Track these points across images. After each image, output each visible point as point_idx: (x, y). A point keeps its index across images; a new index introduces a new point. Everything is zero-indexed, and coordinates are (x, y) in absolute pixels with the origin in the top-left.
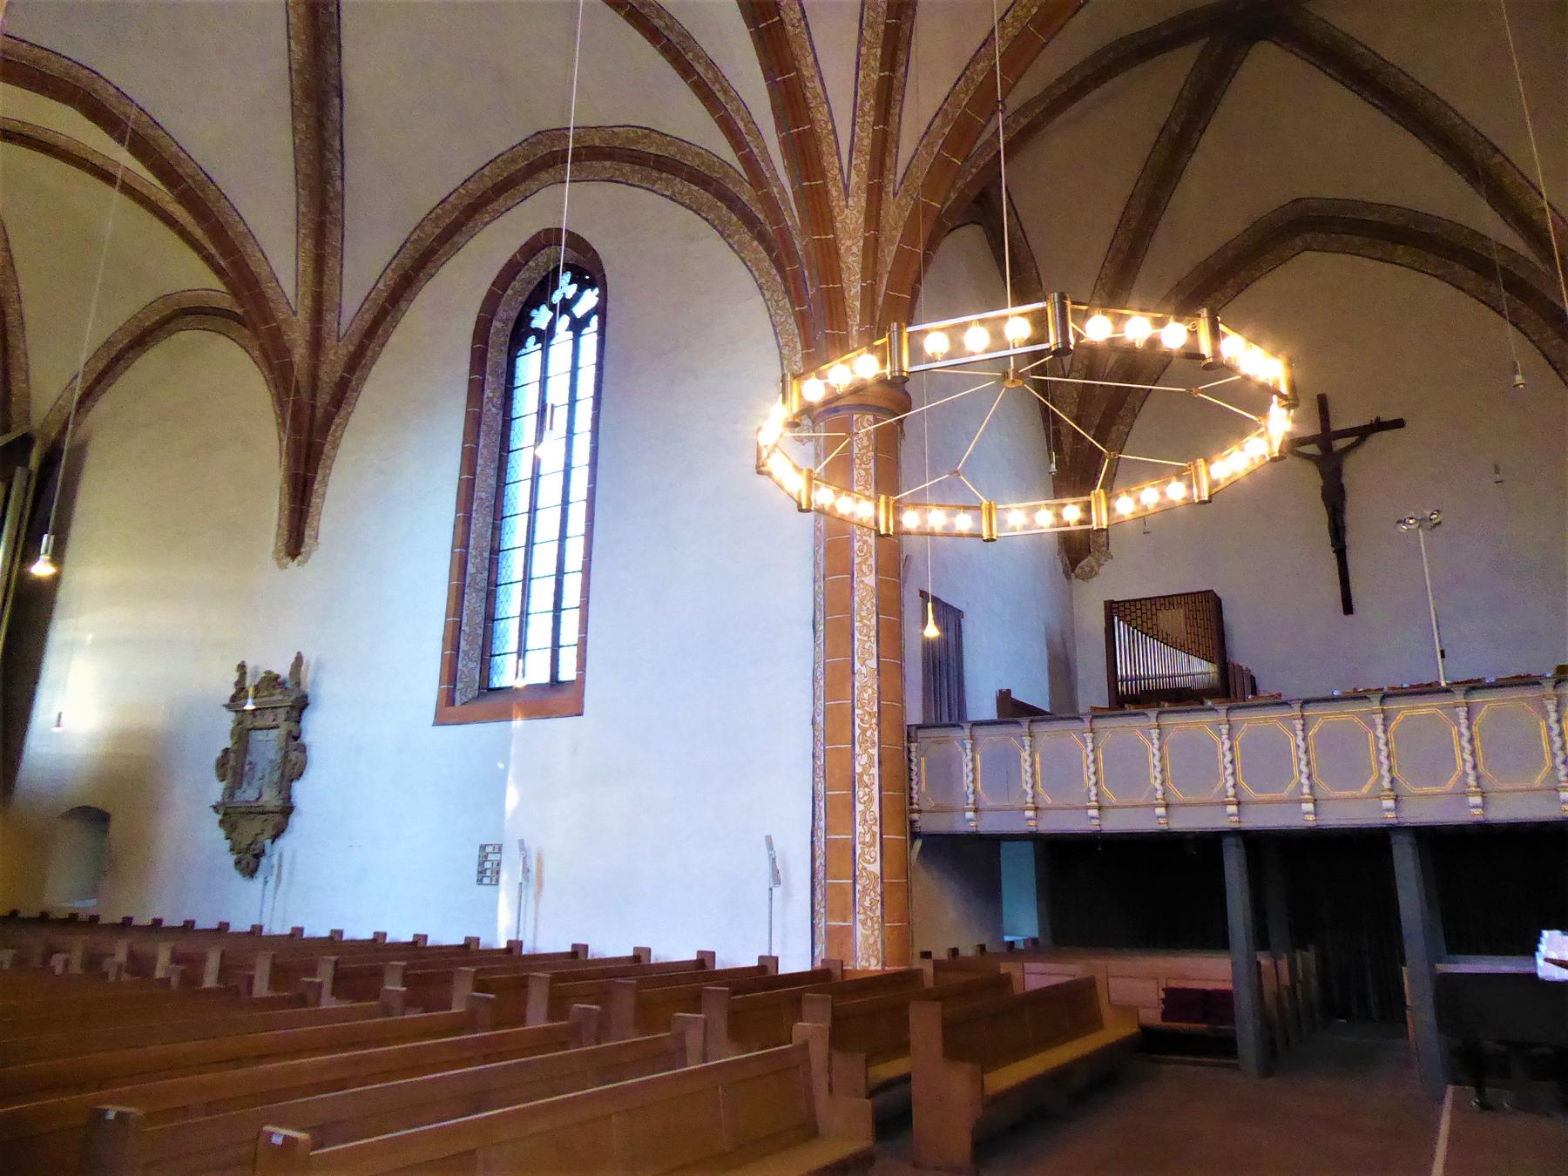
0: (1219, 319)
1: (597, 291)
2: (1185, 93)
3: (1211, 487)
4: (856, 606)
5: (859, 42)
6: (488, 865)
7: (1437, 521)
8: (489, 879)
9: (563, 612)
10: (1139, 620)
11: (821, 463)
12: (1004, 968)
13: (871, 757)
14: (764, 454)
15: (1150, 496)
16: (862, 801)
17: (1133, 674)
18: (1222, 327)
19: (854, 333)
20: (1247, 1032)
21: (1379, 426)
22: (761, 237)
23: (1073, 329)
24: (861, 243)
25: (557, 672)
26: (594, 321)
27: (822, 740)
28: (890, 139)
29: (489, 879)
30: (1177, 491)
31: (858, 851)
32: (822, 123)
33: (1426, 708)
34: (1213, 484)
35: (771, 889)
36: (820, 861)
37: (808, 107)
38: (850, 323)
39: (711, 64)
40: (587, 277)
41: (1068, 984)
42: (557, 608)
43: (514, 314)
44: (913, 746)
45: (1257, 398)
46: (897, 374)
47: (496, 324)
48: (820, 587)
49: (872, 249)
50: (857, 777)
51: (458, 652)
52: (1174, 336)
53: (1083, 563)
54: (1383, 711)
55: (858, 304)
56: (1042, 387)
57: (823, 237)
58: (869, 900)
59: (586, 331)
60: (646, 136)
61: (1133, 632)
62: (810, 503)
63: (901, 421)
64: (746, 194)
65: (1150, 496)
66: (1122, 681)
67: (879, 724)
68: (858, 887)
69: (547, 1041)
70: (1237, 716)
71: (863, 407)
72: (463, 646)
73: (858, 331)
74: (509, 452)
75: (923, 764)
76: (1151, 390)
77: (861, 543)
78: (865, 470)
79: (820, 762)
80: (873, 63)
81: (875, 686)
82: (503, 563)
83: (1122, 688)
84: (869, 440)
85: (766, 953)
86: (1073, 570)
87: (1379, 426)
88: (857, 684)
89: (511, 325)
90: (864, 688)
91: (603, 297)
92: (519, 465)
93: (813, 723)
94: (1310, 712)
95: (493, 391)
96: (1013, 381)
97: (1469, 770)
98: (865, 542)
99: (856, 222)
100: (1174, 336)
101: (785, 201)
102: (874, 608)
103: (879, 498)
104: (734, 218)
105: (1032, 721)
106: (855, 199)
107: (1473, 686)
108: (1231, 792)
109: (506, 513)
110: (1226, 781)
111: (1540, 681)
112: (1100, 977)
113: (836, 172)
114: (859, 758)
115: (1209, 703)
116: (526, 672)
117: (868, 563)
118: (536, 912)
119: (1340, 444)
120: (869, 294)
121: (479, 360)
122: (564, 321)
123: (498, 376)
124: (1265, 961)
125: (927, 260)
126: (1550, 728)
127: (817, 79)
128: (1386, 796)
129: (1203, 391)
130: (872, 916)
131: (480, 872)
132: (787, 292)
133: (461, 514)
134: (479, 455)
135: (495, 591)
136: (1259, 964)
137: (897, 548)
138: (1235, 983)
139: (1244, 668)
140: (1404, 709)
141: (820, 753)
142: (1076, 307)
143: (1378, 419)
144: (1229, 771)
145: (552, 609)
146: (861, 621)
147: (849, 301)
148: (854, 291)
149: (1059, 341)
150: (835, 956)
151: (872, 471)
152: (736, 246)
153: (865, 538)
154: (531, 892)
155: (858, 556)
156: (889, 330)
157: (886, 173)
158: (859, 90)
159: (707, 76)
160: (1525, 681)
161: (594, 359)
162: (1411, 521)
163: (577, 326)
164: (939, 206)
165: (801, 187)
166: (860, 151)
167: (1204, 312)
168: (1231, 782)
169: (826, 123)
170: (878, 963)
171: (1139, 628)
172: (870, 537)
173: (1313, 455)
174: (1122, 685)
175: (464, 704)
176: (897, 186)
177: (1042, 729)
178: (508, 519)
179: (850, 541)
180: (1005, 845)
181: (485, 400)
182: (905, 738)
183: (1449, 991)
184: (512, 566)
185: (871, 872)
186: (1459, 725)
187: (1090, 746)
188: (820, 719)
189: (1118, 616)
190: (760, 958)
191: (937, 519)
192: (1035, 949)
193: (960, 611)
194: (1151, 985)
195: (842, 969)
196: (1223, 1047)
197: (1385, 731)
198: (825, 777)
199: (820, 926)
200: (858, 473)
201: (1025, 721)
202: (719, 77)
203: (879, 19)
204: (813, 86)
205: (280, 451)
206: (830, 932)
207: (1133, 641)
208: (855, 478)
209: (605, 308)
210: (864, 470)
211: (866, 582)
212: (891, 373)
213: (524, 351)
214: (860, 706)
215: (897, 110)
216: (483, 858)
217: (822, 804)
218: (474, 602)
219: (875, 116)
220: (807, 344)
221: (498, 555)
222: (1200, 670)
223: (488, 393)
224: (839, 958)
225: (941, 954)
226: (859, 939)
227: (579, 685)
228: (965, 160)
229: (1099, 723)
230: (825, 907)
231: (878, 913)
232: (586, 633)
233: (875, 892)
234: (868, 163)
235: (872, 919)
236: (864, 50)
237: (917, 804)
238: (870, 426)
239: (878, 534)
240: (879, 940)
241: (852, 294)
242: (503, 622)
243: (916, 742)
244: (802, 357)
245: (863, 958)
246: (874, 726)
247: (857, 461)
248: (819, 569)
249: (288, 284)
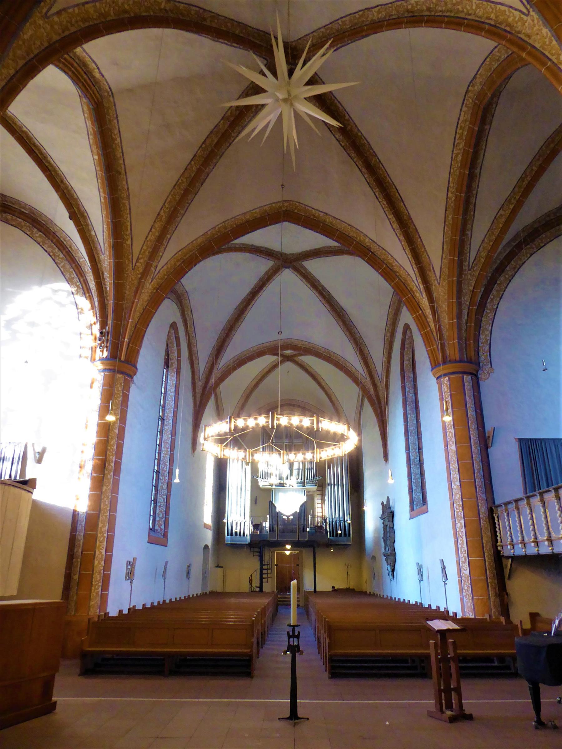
13: (461, 524)
51: (412, 490)
67: (463, 509)
68: (463, 581)
72: (414, 487)
81: (460, 493)
88: (454, 493)
90: (456, 494)
98: (450, 432)
113: (415, 287)
185: (465, 574)
231: (470, 592)
233: (468, 583)
246: (461, 510)
249: (361, 371)
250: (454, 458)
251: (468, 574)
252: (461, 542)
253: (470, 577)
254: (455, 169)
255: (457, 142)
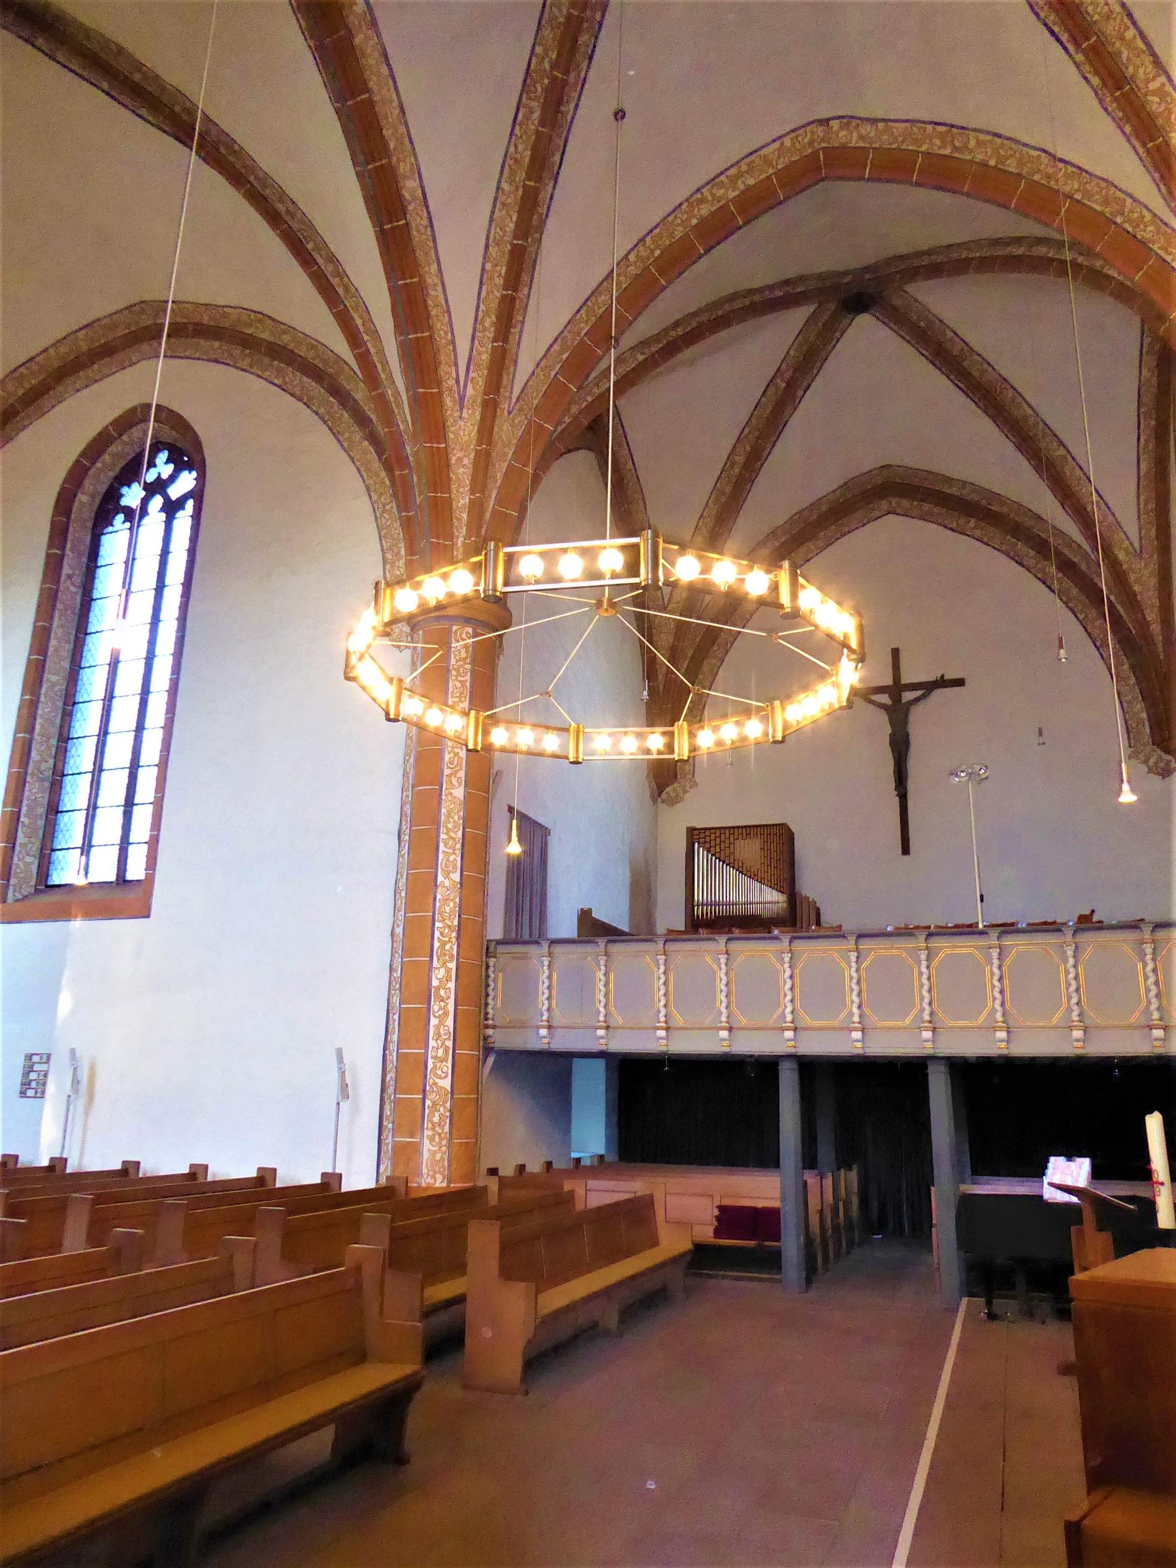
0: (799, 571)
1: (194, 474)
2: (792, 353)
3: (785, 728)
4: (443, 818)
5: (484, 258)
6: (33, 1076)
7: (984, 776)
8: (34, 1090)
9: (135, 807)
10: (718, 847)
11: (416, 670)
12: (567, 1186)
13: (448, 971)
14: (353, 660)
15: (729, 731)
16: (437, 1015)
17: (705, 898)
18: (801, 580)
19: (460, 544)
20: (791, 1245)
21: (942, 683)
22: (373, 439)
23: (663, 564)
24: (472, 456)
25: (125, 870)
26: (190, 504)
27: (400, 952)
28: (508, 357)
29: (34, 1090)
30: (754, 729)
31: (430, 1065)
32: (442, 333)
33: (965, 947)
34: (786, 726)
35: (338, 1104)
36: (390, 1075)
37: (428, 317)
38: (456, 534)
39: (332, 258)
40: (186, 459)
41: (628, 1201)
42: (129, 804)
43: (103, 488)
44: (492, 961)
45: (832, 647)
46: (490, 592)
47: (82, 498)
48: (407, 796)
49: (483, 462)
50: (433, 990)
51: (14, 844)
52: (757, 583)
53: (668, 789)
54: (927, 948)
55: (465, 516)
56: (640, 620)
57: (435, 445)
58: (437, 1114)
59: (180, 514)
60: (260, 321)
61: (711, 859)
62: (398, 714)
63: (501, 636)
64: (360, 393)
65: (729, 731)
66: (698, 905)
67: (458, 938)
68: (428, 1103)
69: (84, 1268)
70: (799, 945)
71: (467, 621)
72: (21, 838)
73: (464, 543)
74: (87, 634)
75: (500, 980)
76: (740, 632)
77: (452, 755)
78: (461, 682)
79: (397, 974)
80: (497, 280)
81: (457, 900)
82: (73, 751)
83: (698, 911)
84: (467, 652)
85: (330, 1170)
86: (660, 795)
87: (942, 683)
88: (439, 896)
89: (98, 501)
90: (446, 900)
91: (201, 479)
92: (96, 649)
93: (392, 935)
94: (865, 945)
95: (71, 567)
96: (606, 610)
97: (998, 1007)
98: (456, 754)
99: (469, 435)
100: (757, 583)
101: (400, 405)
102: (461, 821)
103: (690, 751)
104: (346, 415)
105: (609, 941)
106: (470, 412)
107: (1008, 928)
108: (789, 1018)
109: (79, 698)
110: (786, 1007)
111: (1063, 929)
112: (659, 1196)
113: (452, 382)
114: (437, 971)
115: (776, 932)
116: (90, 870)
117: (458, 776)
118: (85, 1127)
119: (908, 696)
120: (477, 508)
121: (59, 534)
122: (157, 502)
123: (80, 555)
124: (811, 1178)
125: (536, 479)
126: (1067, 972)
127: (439, 288)
128: (925, 1027)
129: (781, 638)
130: (440, 1131)
131: (23, 1084)
132: (395, 495)
133: (27, 697)
134: (53, 635)
135: (61, 782)
136: (805, 1183)
137: (489, 763)
138: (783, 1199)
139: (811, 900)
140: (946, 947)
141: (397, 965)
142: (668, 545)
143: (942, 676)
144: (789, 998)
145: (123, 803)
146: (447, 834)
147: (456, 514)
148: (462, 502)
149: (650, 576)
150: (401, 1172)
151: (468, 684)
152: (345, 444)
153: (456, 750)
154: (81, 1103)
155: (448, 767)
156: (486, 549)
157: (502, 390)
158: (481, 305)
159: (328, 269)
160: (1050, 927)
161: (186, 544)
162: (962, 774)
163: (171, 508)
164: (552, 429)
165: (416, 393)
166: (479, 366)
167: (786, 564)
168: (789, 1009)
169: (446, 333)
170: (444, 1178)
171: (717, 855)
172: (462, 749)
173: (884, 704)
174: (698, 909)
175: (17, 901)
176: (512, 404)
177: (617, 949)
178: (80, 705)
179: (439, 754)
180: (578, 1065)
181: (63, 578)
182: (484, 952)
183: (968, 1206)
184: (82, 756)
185: (441, 1088)
186: (992, 964)
187: (662, 969)
188: (399, 930)
189: (699, 843)
190: (324, 1175)
191: (525, 737)
192: (601, 1167)
193: (546, 828)
194: (706, 1201)
195: (407, 1187)
196: (772, 1261)
197: (928, 967)
198: (400, 990)
199: (387, 1141)
200: (454, 684)
201: (602, 942)
202: (341, 274)
203: (505, 238)
204: (435, 293)
205: (643, 670)
206: (398, 1149)
207: (711, 869)
208: (451, 689)
209: (202, 492)
210: (460, 681)
211: (454, 794)
212: (485, 591)
213: (110, 529)
214: (440, 919)
215: (518, 329)
216: (28, 1070)
217: (396, 1017)
218: (35, 792)
219: (496, 331)
220: (411, 550)
221: (67, 743)
222: (770, 899)
223: (66, 570)
224: (404, 1175)
225: (508, 1171)
226: (426, 1154)
227: (146, 885)
228: (580, 388)
229: (671, 947)
230: (393, 1123)
231: (447, 1129)
232: (159, 830)
233: (445, 1107)
234: (484, 377)
235: (439, 1135)
236: (488, 266)
237: (493, 1020)
238: (469, 638)
239: (468, 750)
240: (446, 1157)
241: (459, 505)
242: (67, 815)
243: (495, 957)
244: (405, 562)
245: (428, 1175)
246: (454, 940)
247: (454, 673)
248: (408, 780)
250: (456, 818)
251: (449, 1088)
252: (441, 1012)
253: (452, 1094)
254: (679, 221)
255: (723, 178)
